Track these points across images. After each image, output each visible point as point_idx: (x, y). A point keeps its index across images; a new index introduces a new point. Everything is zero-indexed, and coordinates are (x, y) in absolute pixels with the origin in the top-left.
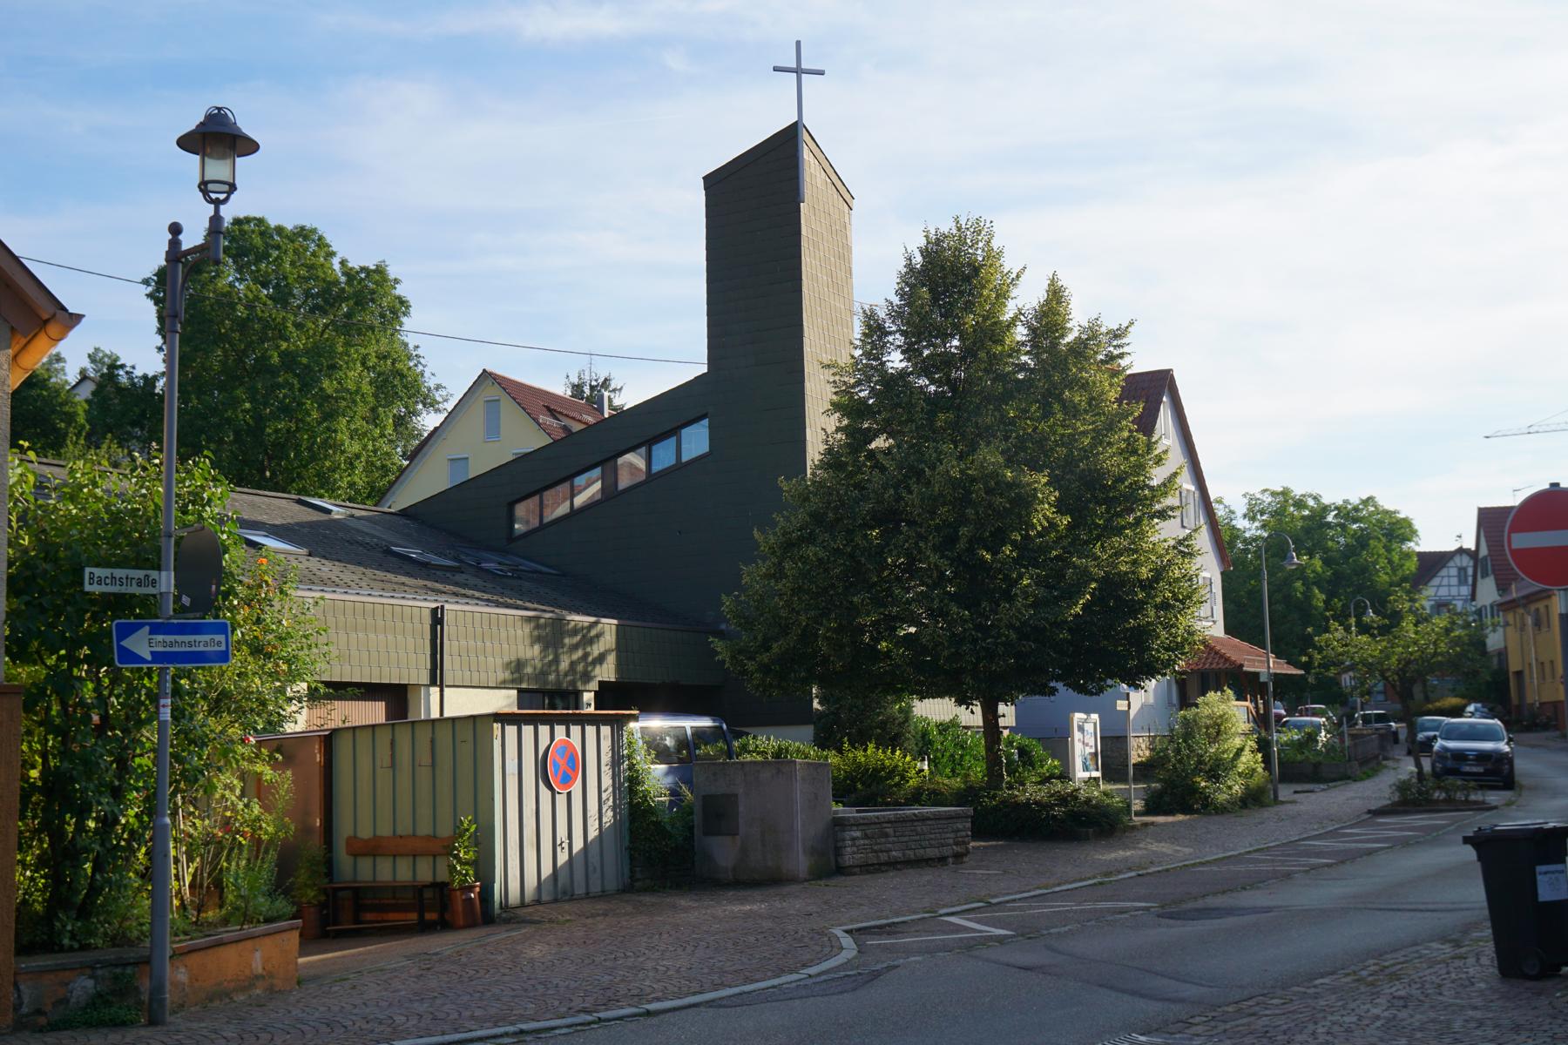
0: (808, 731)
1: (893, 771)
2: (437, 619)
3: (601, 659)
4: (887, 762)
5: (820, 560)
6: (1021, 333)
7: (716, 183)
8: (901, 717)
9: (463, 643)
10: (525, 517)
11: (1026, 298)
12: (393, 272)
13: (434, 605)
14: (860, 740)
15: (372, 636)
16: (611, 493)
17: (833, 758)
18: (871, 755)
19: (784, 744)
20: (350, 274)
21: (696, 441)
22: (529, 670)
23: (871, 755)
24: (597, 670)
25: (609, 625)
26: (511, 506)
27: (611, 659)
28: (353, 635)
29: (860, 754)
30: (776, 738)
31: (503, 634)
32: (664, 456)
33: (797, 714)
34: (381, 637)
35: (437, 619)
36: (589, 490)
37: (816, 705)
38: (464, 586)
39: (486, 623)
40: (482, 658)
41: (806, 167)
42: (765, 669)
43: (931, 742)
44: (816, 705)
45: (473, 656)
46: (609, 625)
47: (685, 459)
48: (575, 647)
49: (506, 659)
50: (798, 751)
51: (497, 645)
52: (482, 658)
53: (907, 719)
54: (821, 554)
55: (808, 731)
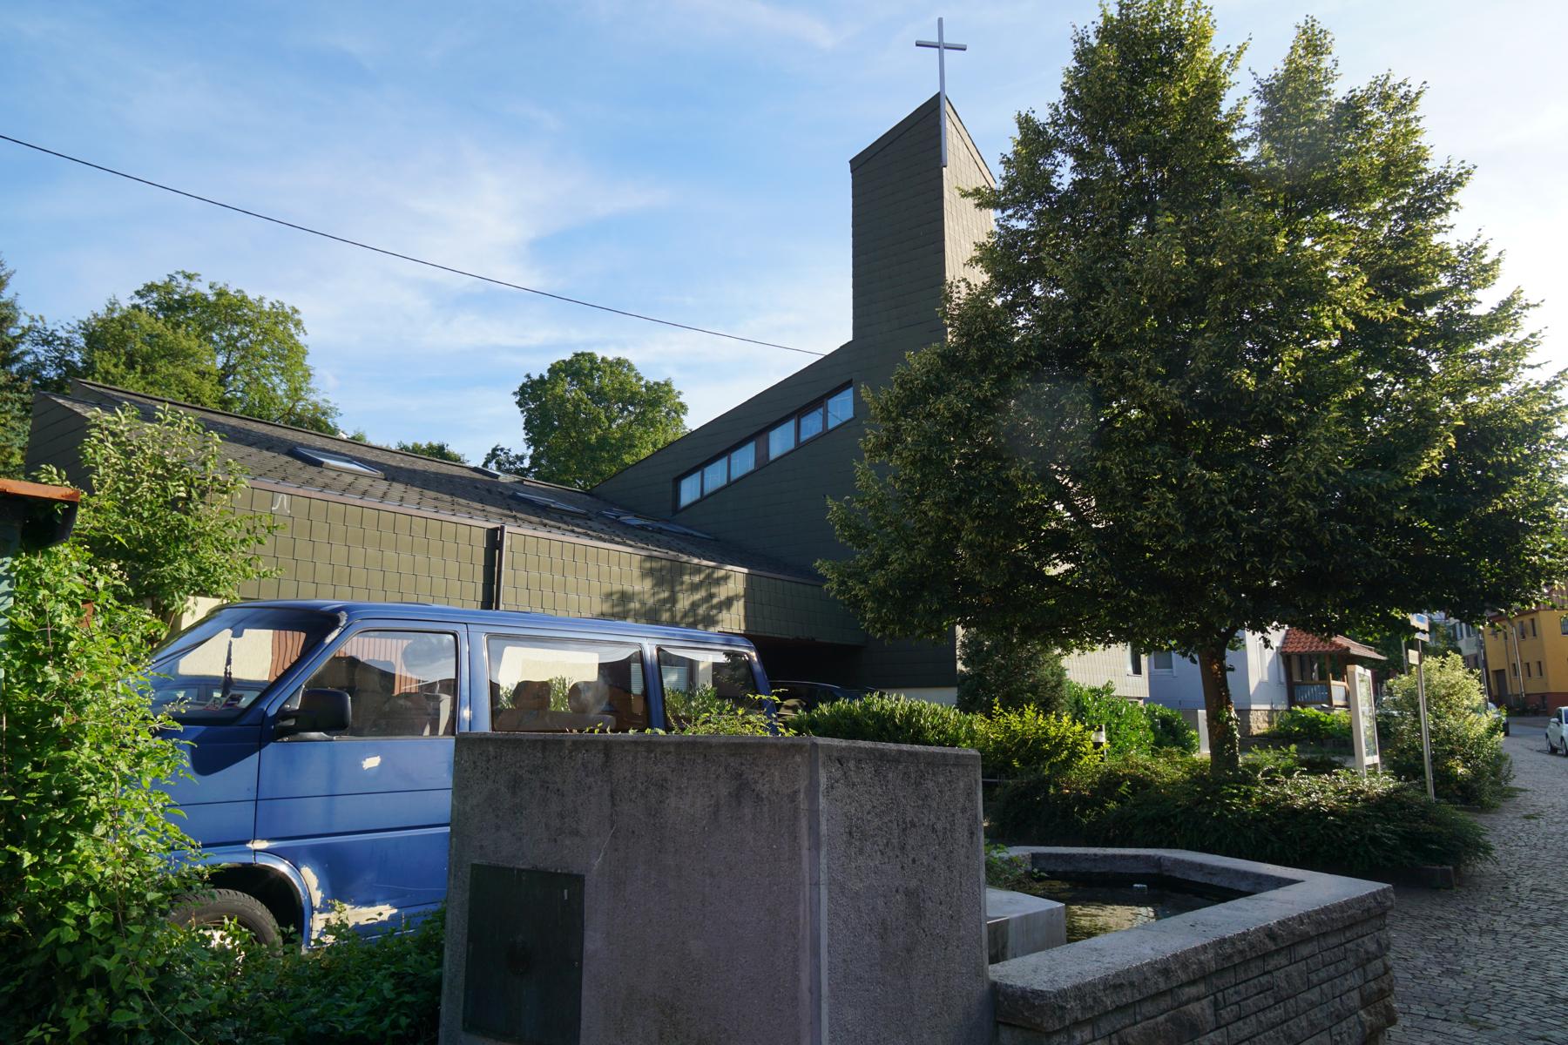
0: (952, 693)
1: (1060, 744)
2: (494, 541)
3: (728, 603)
4: (1052, 732)
5: (957, 416)
6: (1252, 112)
7: (862, 165)
8: (1053, 681)
9: (534, 574)
10: (689, 491)
11: (1267, 58)
12: (676, 387)
13: (491, 526)
14: (1014, 702)
15: (390, 554)
16: (763, 462)
17: (979, 724)
18: (1027, 721)
19: (916, 705)
20: (648, 388)
21: (841, 408)
22: (635, 605)
23: (1027, 721)
24: (724, 615)
25: (736, 578)
26: (678, 480)
27: (739, 607)
28: (358, 551)
29: (1013, 718)
30: (907, 697)
31: (593, 570)
32: (812, 425)
33: (935, 675)
34: (405, 556)
35: (494, 541)
36: (744, 461)
37: (960, 666)
38: (590, 528)
39: (568, 557)
40: (560, 595)
41: (949, 136)
42: (880, 596)
43: (1085, 709)
44: (960, 666)
45: (547, 592)
46: (736, 578)
47: (831, 426)
48: (694, 588)
49: (606, 588)
50: (935, 713)
51: (582, 580)
52: (560, 595)
53: (1059, 684)
54: (959, 405)
55: (952, 693)
